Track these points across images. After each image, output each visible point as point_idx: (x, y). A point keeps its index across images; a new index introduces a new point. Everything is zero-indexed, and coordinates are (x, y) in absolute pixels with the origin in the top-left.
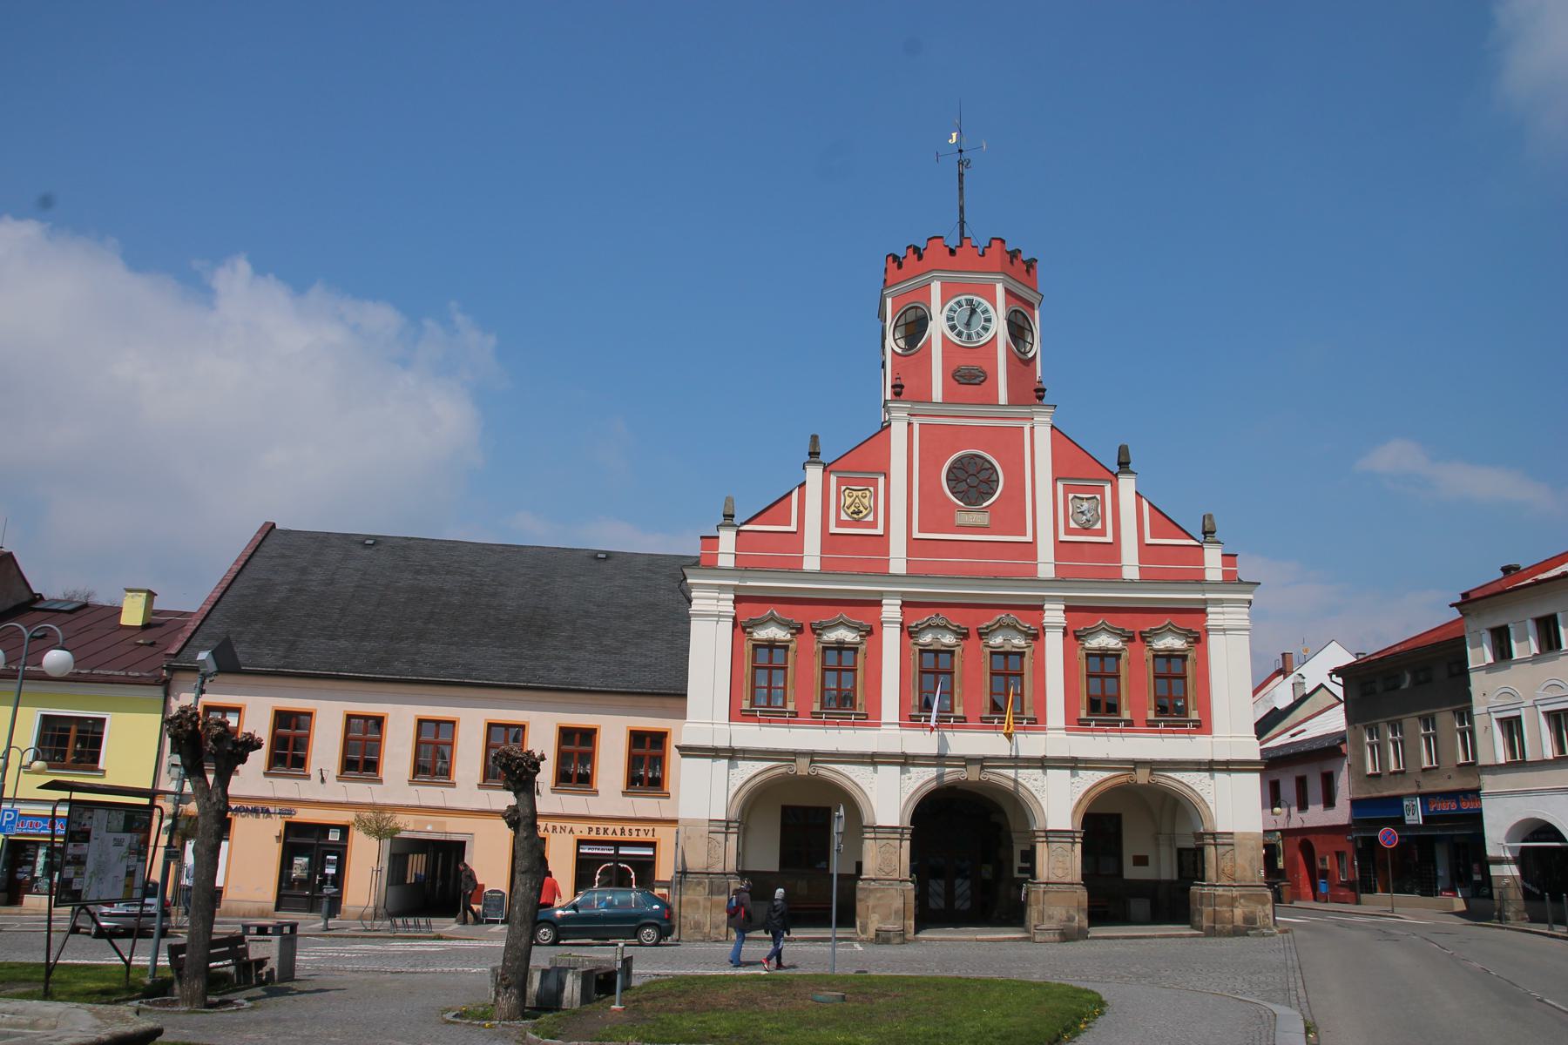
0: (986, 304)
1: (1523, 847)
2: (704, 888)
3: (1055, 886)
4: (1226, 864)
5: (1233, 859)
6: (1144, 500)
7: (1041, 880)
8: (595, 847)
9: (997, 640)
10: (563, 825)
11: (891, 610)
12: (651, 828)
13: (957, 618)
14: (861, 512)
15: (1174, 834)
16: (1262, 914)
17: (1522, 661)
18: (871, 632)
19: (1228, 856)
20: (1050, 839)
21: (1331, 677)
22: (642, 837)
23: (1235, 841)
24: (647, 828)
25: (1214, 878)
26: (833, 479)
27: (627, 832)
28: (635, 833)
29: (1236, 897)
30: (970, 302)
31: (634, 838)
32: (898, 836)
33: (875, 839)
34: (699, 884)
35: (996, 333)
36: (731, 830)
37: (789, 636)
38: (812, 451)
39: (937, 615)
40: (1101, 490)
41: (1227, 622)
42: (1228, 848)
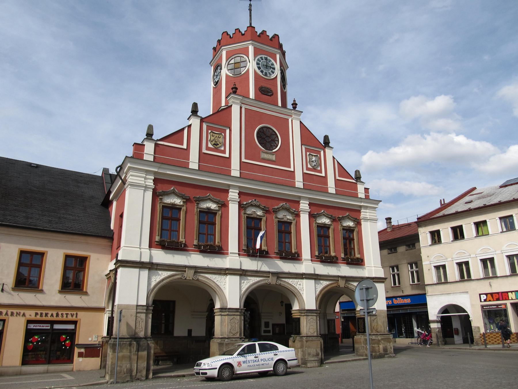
0: (273, 61)
1: (442, 316)
3: (311, 338)
4: (374, 324)
5: (377, 322)
6: (335, 159)
8: (38, 325)
9: (281, 215)
10: (18, 311)
11: (233, 195)
12: (75, 313)
13: (263, 203)
14: (218, 145)
15: (326, 313)
17: (446, 243)
18: (224, 205)
19: (375, 321)
22: (70, 318)
24: (72, 313)
26: (205, 126)
27: (60, 315)
28: (65, 316)
29: (380, 340)
30: (266, 59)
31: (65, 318)
35: (277, 75)
37: (182, 203)
38: (194, 110)
39: (255, 200)
40: (319, 153)
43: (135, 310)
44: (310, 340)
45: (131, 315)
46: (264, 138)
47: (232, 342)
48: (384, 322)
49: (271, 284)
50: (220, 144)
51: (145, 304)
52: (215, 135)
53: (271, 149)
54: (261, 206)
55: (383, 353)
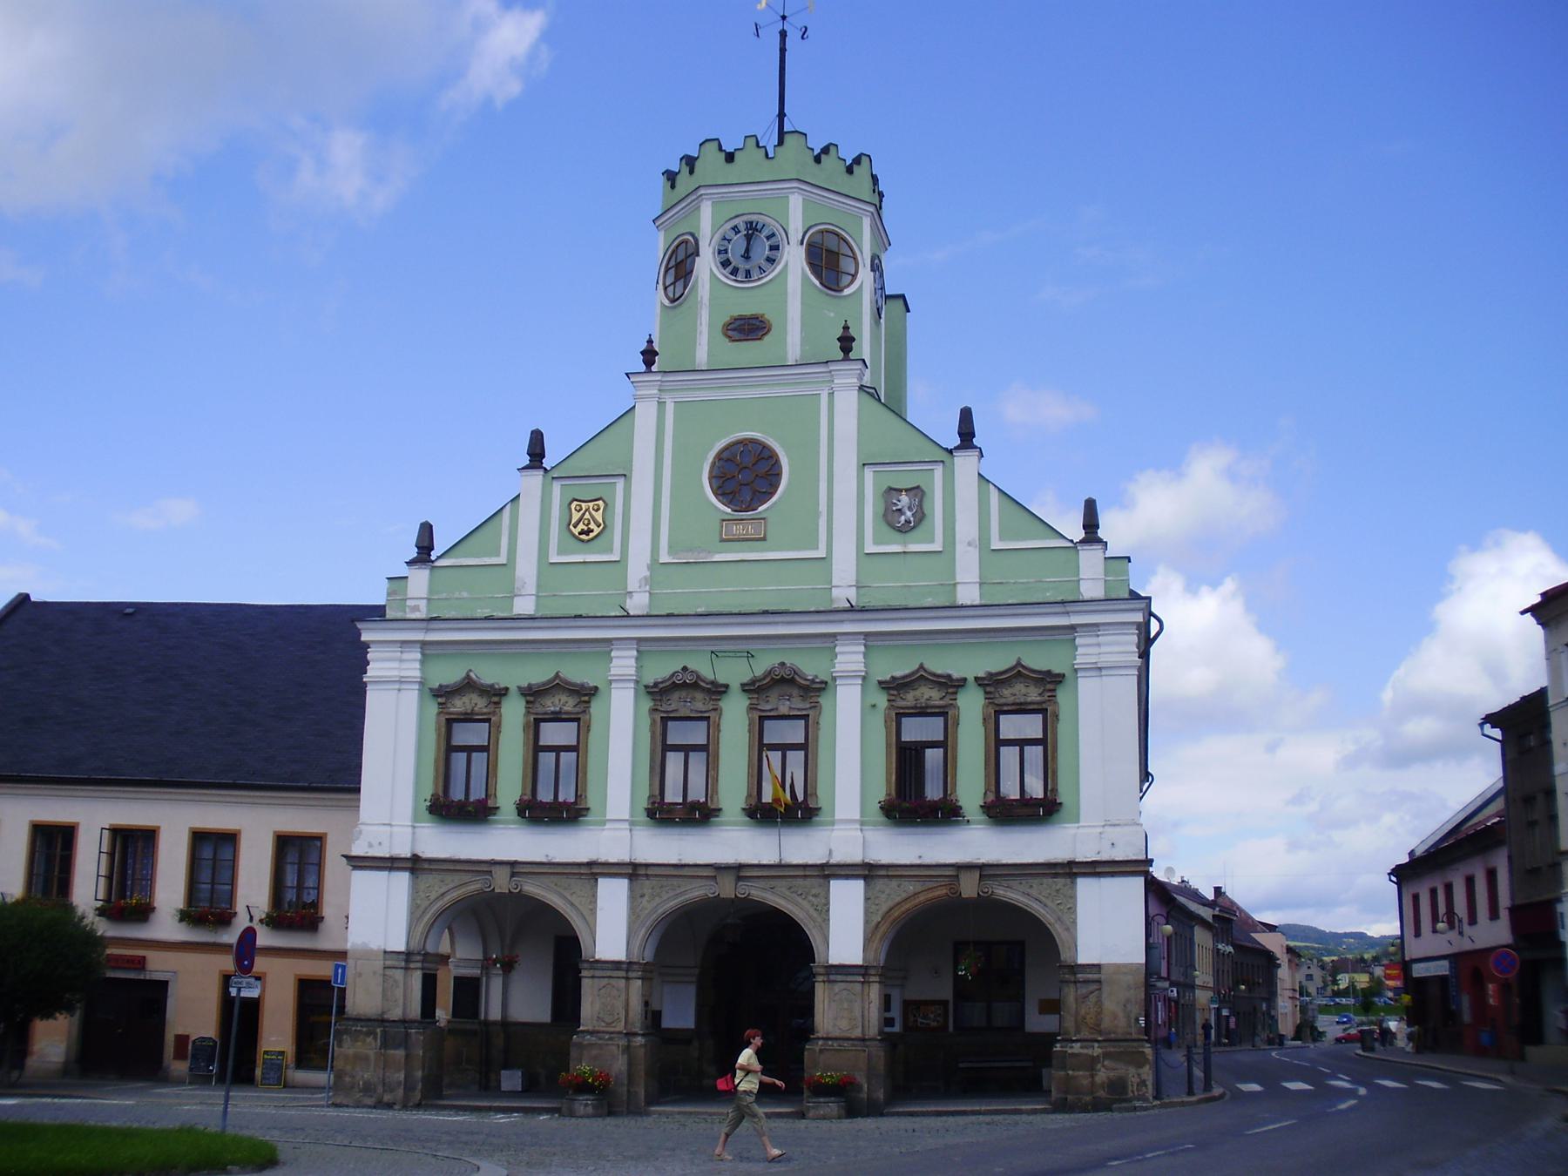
2: (375, 1038)
5: (1099, 1003)
7: (820, 1035)
14: (592, 531)
16: (1136, 1080)
19: (1092, 998)
20: (832, 977)
21: (1482, 729)
23: (1103, 977)
25: (1072, 1031)
32: (622, 974)
33: (593, 977)
34: (368, 1034)
36: (412, 965)
41: (1104, 658)
42: (1093, 987)
43: (382, 962)
44: (831, 1050)
45: (375, 973)
46: (734, 476)
47: (600, 1042)
48: (1128, 1001)
49: (721, 896)
50: (599, 527)
51: (402, 948)
52: (583, 505)
53: (754, 507)
54: (702, 684)
55: (1106, 1098)
